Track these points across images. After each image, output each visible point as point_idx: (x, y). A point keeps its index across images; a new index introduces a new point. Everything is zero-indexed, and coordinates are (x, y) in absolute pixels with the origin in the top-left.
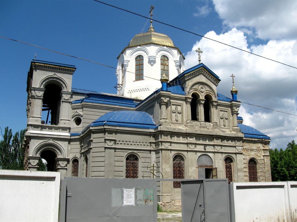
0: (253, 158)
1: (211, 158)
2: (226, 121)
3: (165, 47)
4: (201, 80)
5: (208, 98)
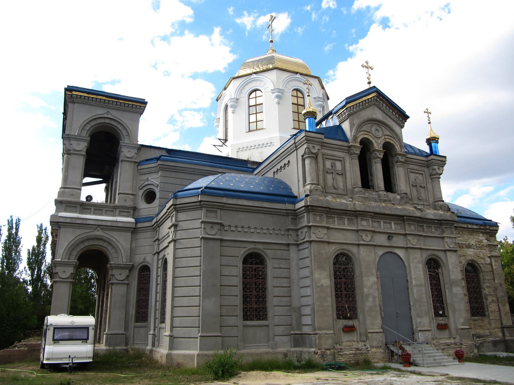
0: (472, 260)
1: (401, 259)
2: (422, 190)
3: (298, 76)
4: (374, 116)
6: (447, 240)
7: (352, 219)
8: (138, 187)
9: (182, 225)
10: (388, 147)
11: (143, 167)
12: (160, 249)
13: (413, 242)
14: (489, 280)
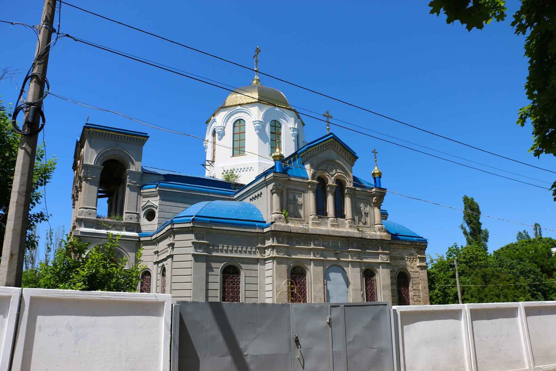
5: (340, 183)
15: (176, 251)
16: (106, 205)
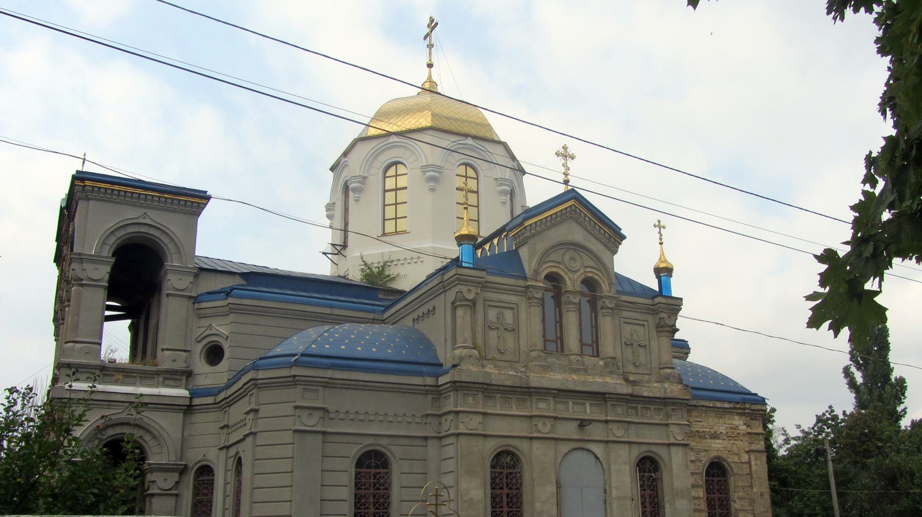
0: (718, 457)
2: (642, 351)
3: (469, 141)
4: (570, 238)
6: (672, 428)
7: (524, 400)
8: (194, 337)
9: (264, 411)
10: (590, 284)
11: (204, 305)
12: (231, 442)
13: (618, 432)
14: (743, 487)
15: (261, 425)
16: (127, 336)
